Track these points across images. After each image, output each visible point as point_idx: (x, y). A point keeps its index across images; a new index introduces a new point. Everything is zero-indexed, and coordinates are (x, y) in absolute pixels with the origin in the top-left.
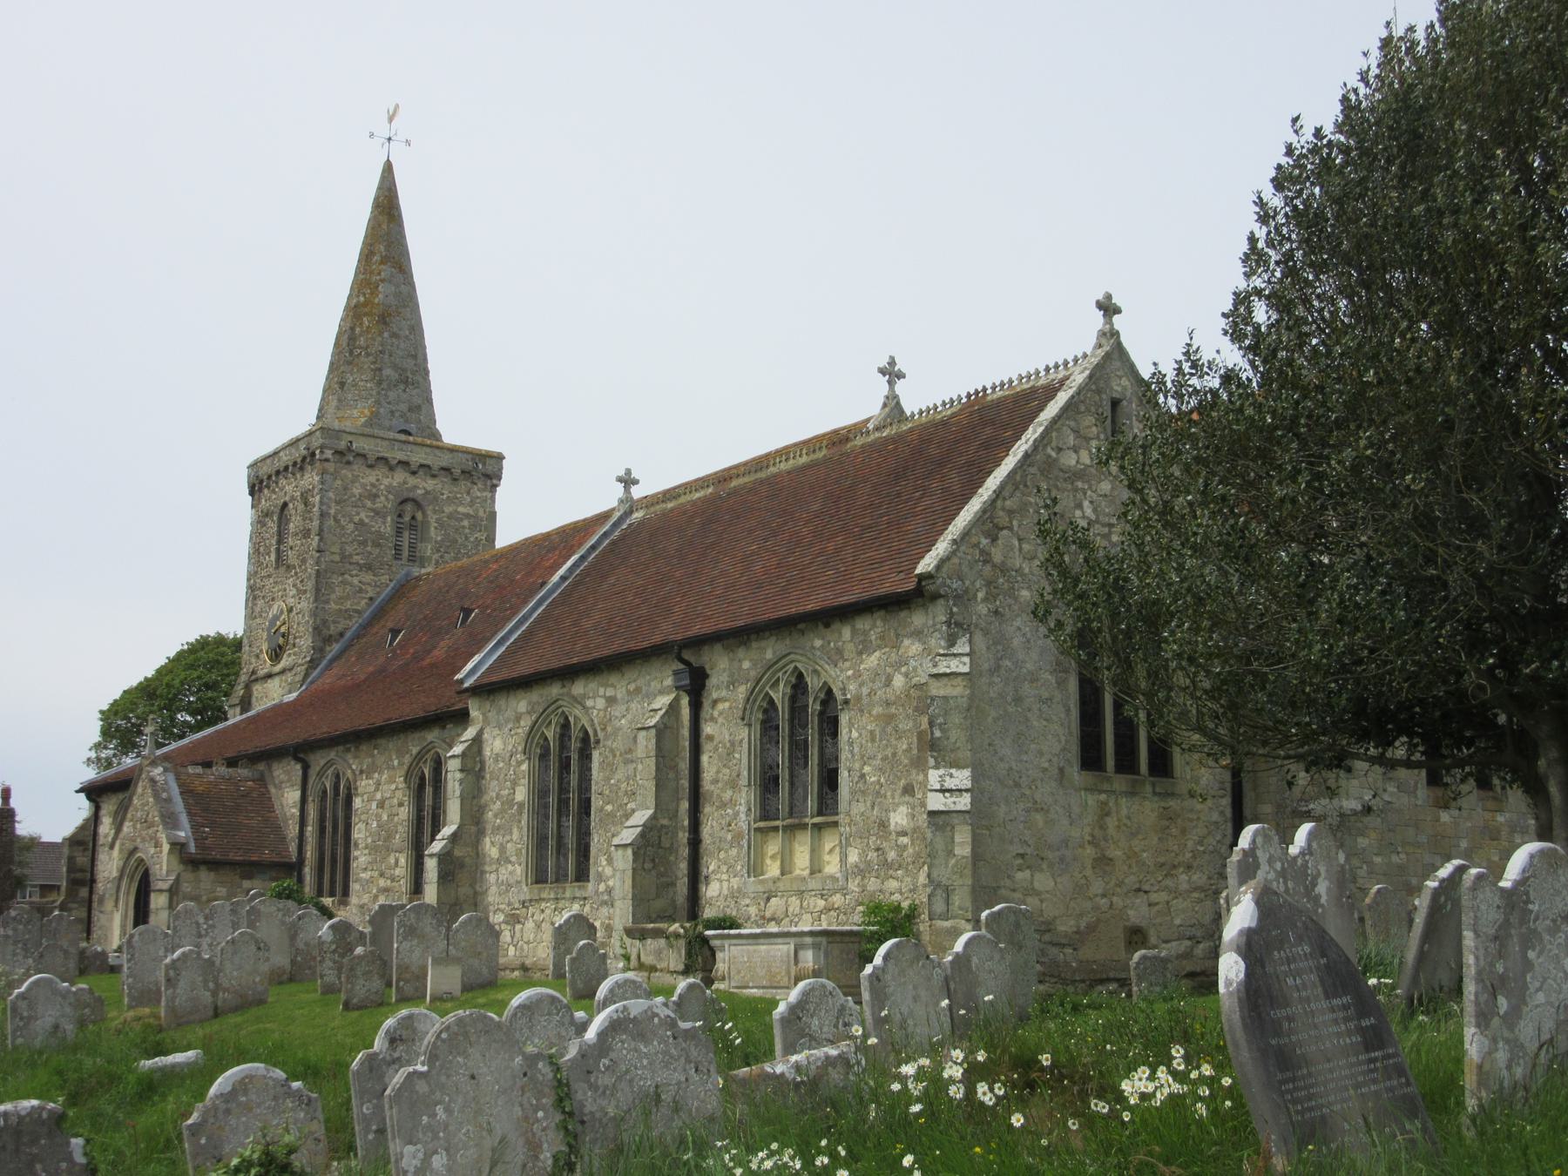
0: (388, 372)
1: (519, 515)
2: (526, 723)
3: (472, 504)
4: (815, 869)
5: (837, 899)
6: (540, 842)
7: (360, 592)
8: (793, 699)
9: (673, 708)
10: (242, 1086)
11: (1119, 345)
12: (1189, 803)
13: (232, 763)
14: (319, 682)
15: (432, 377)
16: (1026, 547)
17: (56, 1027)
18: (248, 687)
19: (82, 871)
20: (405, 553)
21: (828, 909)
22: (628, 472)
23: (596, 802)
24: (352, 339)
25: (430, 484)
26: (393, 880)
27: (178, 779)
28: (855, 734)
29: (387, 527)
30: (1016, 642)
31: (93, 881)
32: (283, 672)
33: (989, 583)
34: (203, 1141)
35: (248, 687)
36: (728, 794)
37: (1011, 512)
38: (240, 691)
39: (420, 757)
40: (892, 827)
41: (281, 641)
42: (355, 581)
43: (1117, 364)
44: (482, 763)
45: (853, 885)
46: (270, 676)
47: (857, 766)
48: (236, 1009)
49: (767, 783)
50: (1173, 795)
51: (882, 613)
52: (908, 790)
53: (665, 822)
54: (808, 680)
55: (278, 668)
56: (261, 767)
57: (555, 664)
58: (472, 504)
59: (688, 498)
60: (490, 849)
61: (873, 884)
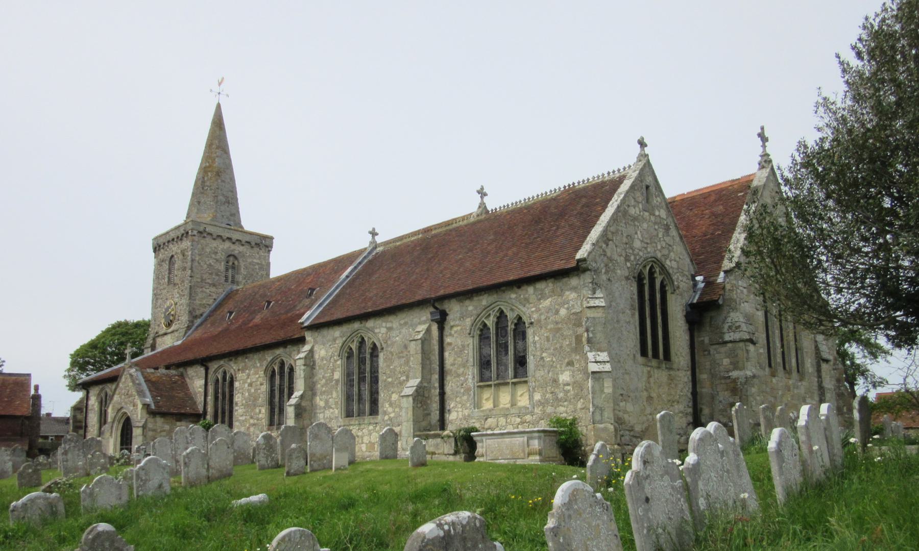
0: (221, 198)
1: (282, 263)
2: (339, 342)
3: (260, 258)
4: (513, 404)
5: (528, 418)
6: (349, 398)
7: (209, 297)
8: (497, 323)
9: (428, 331)
10: (574, 496)
11: (648, 161)
12: (677, 373)
13: (168, 367)
14: (193, 336)
15: (239, 201)
16: (619, 250)
17: (160, 486)
18: (154, 339)
19: (80, 422)
20: (230, 279)
21: (522, 423)
22: (374, 229)
23: (382, 377)
24: (203, 182)
25: (241, 248)
26: (258, 420)
27: (143, 374)
28: (537, 338)
29: (222, 267)
30: (617, 294)
31: (86, 426)
32: (173, 332)
33: (606, 265)
34: (561, 540)
35: (154, 339)
36: (462, 370)
37: (613, 233)
38: (150, 341)
39: (272, 361)
40: (561, 381)
41: (171, 318)
42: (208, 291)
43: (647, 169)
44: (314, 362)
45: (538, 410)
46: (166, 334)
47: (538, 353)
48: (219, 478)
49: (484, 364)
50: (671, 369)
51: (552, 280)
52: (570, 363)
53: (425, 384)
54: (508, 314)
55: (170, 330)
56: (181, 370)
57: (357, 312)
58: (260, 258)
59: (408, 240)
60: (320, 402)
61: (549, 409)
